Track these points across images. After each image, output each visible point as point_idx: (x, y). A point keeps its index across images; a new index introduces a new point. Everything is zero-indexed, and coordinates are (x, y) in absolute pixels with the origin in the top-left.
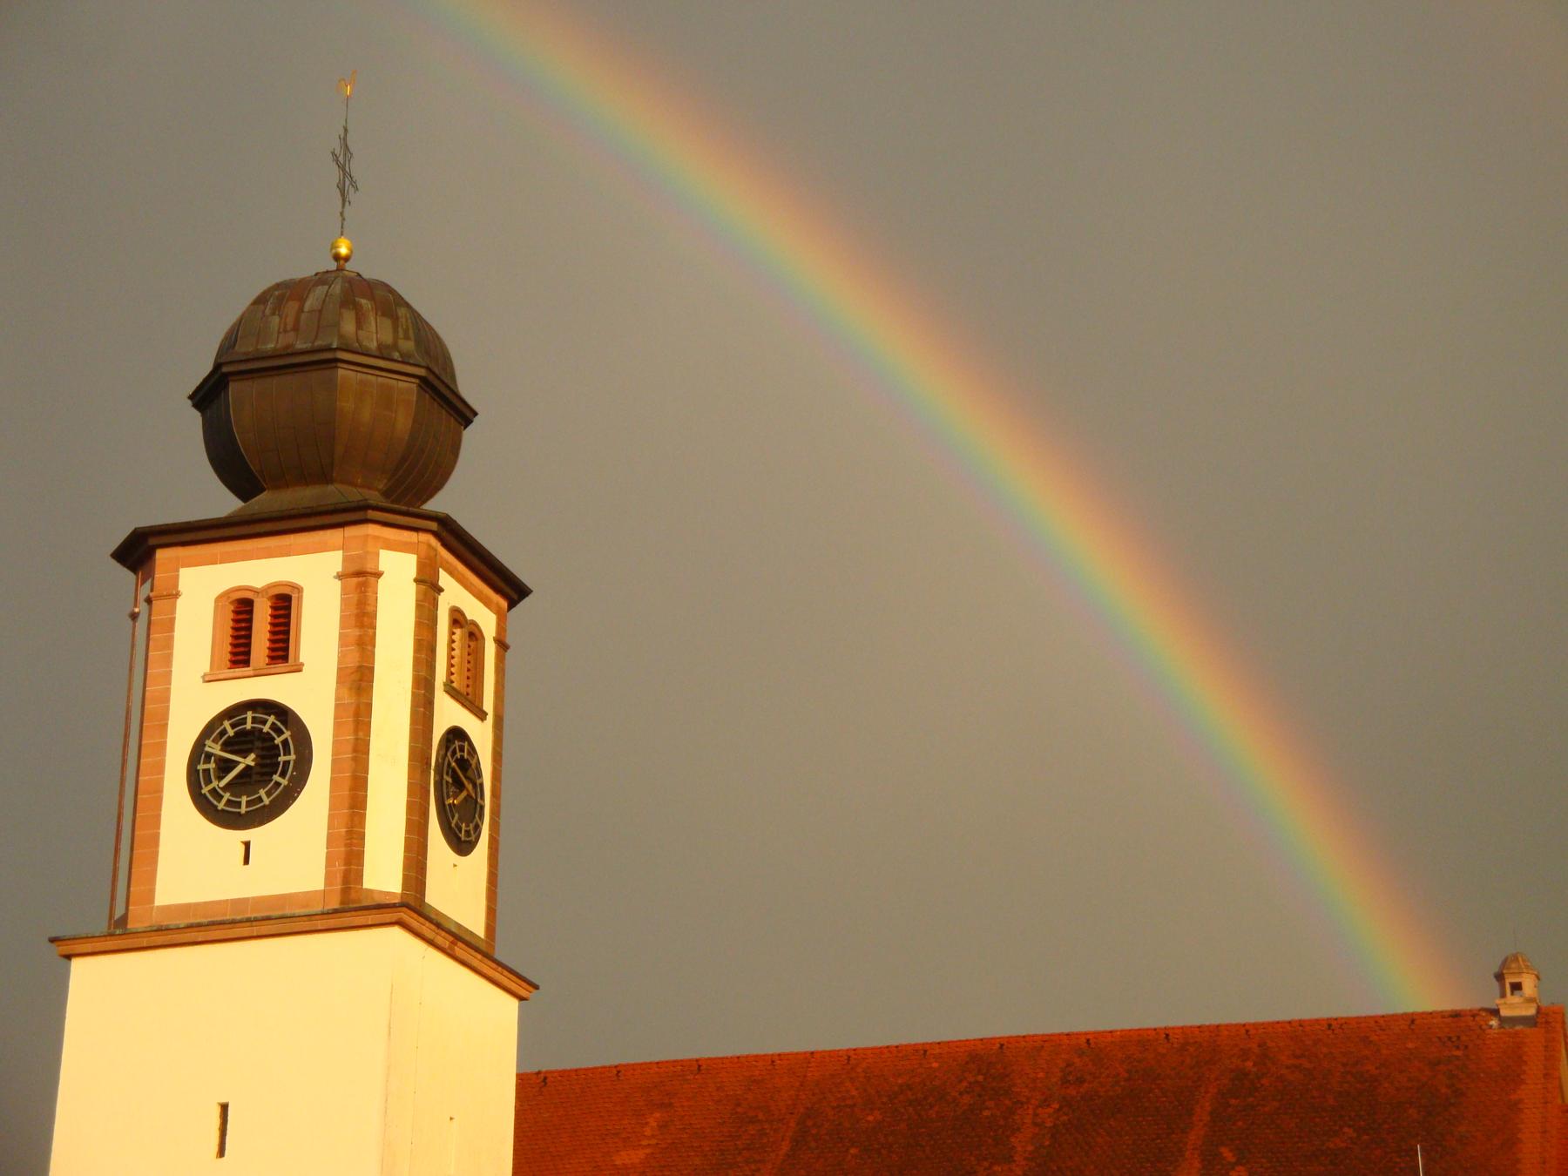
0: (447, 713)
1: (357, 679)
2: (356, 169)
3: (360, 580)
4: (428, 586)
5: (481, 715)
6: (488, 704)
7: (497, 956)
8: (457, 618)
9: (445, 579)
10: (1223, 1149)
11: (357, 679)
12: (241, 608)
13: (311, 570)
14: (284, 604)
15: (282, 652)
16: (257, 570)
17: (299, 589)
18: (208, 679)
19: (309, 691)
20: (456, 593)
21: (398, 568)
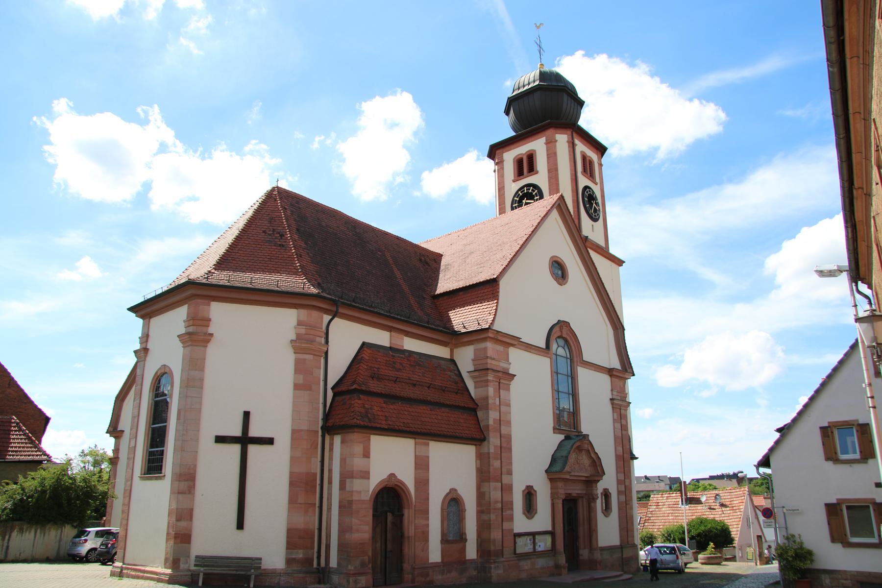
0: (583, 181)
1: (553, 171)
2: (543, 46)
3: (551, 144)
4: (572, 146)
5: (596, 184)
6: (598, 180)
7: (612, 251)
8: (584, 157)
9: (577, 142)
10: (566, 419)
11: (553, 171)
12: (519, 162)
13: (538, 145)
14: (531, 157)
15: (532, 169)
16: (522, 150)
17: (535, 151)
18: (514, 181)
19: (540, 179)
20: (581, 147)
21: (562, 139)
